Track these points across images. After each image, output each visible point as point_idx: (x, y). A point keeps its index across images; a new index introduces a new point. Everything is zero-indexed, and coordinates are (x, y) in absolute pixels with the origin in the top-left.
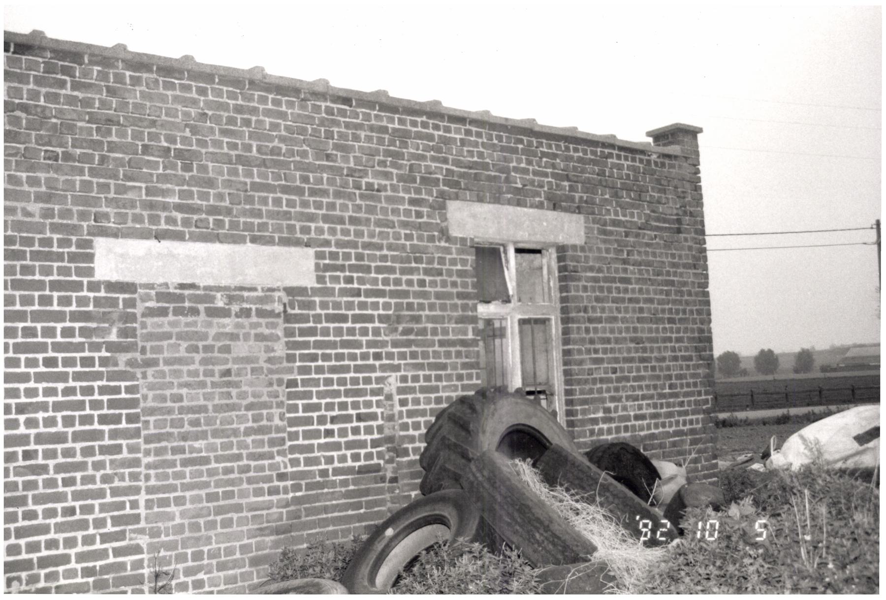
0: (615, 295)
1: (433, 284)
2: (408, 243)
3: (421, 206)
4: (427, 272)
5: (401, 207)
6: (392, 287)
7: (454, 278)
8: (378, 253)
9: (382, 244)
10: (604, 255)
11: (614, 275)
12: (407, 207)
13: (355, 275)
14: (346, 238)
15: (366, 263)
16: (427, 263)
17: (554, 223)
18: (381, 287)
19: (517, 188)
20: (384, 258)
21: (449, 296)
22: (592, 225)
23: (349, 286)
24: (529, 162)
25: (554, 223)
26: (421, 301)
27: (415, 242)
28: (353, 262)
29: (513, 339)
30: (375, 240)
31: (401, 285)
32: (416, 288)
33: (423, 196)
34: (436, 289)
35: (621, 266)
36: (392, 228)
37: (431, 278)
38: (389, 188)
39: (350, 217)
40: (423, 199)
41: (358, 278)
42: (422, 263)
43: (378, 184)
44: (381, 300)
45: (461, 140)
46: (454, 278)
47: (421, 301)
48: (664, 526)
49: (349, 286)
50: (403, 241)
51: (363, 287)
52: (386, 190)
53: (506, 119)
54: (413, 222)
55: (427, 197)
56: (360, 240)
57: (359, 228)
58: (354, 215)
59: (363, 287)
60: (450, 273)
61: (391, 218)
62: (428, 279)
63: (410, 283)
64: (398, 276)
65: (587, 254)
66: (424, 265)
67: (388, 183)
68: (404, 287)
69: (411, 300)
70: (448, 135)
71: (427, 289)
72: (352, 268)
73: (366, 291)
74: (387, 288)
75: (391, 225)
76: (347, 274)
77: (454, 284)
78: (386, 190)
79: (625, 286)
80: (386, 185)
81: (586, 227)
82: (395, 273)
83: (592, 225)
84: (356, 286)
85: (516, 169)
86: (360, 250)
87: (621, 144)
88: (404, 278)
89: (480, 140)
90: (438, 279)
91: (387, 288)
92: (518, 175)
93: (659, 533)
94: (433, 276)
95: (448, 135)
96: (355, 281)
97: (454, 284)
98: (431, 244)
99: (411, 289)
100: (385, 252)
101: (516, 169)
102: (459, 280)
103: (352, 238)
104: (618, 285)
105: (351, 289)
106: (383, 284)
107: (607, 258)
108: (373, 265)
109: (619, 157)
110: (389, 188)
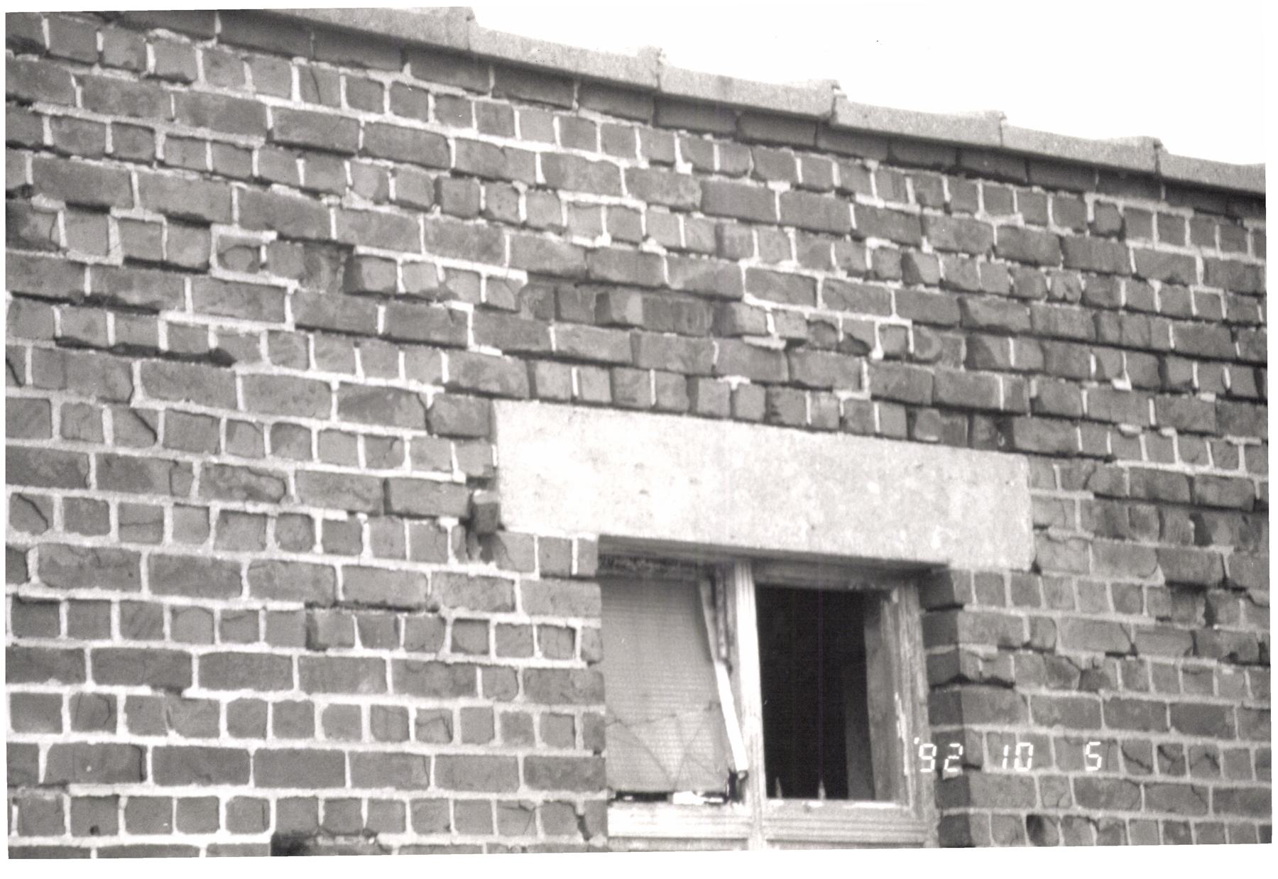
0: (1158, 776)
1: (438, 725)
2: (339, 562)
3: (389, 422)
4: (411, 678)
5: (315, 425)
6: (273, 742)
7: (519, 703)
8: (217, 606)
9: (235, 570)
10: (1113, 616)
11: (1153, 695)
12: (335, 421)
13: (121, 692)
14: (88, 542)
15: (170, 645)
16: (410, 647)
17: (910, 482)
18: (226, 740)
19: (767, 350)
20: (240, 624)
21: (499, 774)
22: (1061, 493)
23: (95, 738)
24: (814, 258)
25: (910, 482)
26: (387, 793)
27: (367, 557)
28: (117, 641)
29: (740, 714)
30: (207, 550)
31: (308, 731)
32: (368, 744)
33: (400, 382)
34: (448, 750)
35: (1181, 662)
36: (277, 501)
37: (430, 704)
38: (263, 347)
39: (107, 461)
40: (400, 392)
41: (134, 704)
42: (392, 644)
43: (222, 334)
44: (225, 793)
45: (549, 158)
46: (519, 703)
47: (387, 793)
48: (955, 751)
49: (95, 738)
50: (317, 556)
51: (151, 742)
52: (255, 357)
53: (725, 82)
54: (360, 478)
55: (413, 386)
56: (146, 550)
57: (143, 499)
58: (122, 451)
59: (151, 742)
60: (502, 684)
61: (271, 463)
62: (414, 705)
63: (343, 722)
64: (296, 694)
65: (1044, 611)
66: (401, 654)
67: (258, 327)
68: (320, 741)
69: (347, 791)
70: (499, 141)
71: (412, 746)
72: (110, 667)
73: (164, 754)
74: (252, 745)
75: (273, 489)
76: (89, 686)
77: (517, 728)
78: (255, 357)
79: (1200, 741)
80: (253, 338)
81: (1035, 499)
82: (288, 684)
83: (1061, 493)
84: (123, 735)
85: (760, 281)
86: (145, 594)
87: (1181, 174)
88: (322, 701)
89: (623, 164)
90: (456, 705)
91: (252, 745)
92: (768, 305)
93: (947, 762)
94: (436, 693)
95: (499, 141)
96: (122, 717)
97: (517, 728)
98: (427, 568)
99: (346, 747)
100: (245, 601)
101: (760, 281)
102: (536, 712)
103: (111, 539)
104: (1173, 737)
105: (106, 750)
106: (237, 729)
107: (1123, 628)
108: (197, 650)
109: (1170, 231)
110: (263, 347)
